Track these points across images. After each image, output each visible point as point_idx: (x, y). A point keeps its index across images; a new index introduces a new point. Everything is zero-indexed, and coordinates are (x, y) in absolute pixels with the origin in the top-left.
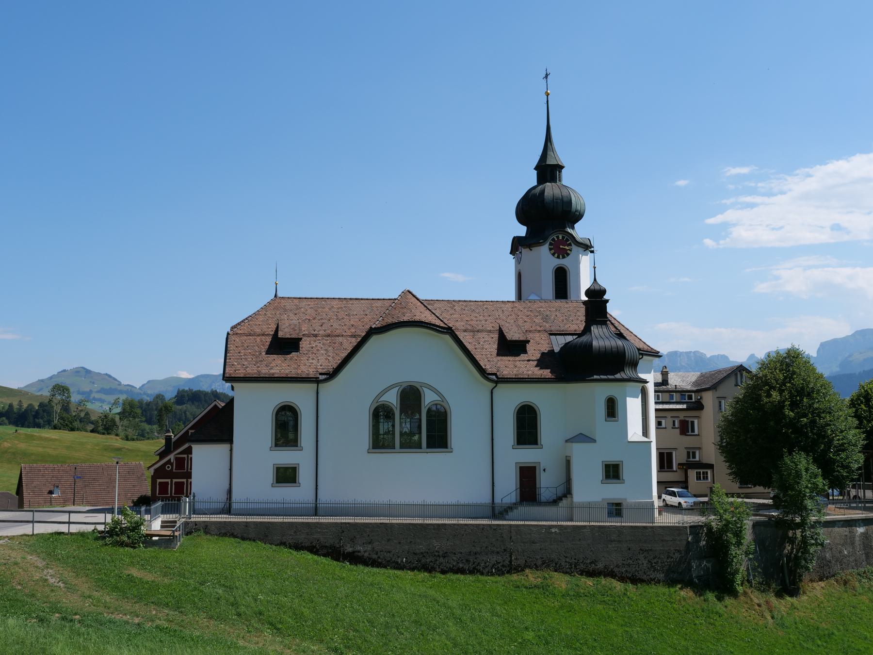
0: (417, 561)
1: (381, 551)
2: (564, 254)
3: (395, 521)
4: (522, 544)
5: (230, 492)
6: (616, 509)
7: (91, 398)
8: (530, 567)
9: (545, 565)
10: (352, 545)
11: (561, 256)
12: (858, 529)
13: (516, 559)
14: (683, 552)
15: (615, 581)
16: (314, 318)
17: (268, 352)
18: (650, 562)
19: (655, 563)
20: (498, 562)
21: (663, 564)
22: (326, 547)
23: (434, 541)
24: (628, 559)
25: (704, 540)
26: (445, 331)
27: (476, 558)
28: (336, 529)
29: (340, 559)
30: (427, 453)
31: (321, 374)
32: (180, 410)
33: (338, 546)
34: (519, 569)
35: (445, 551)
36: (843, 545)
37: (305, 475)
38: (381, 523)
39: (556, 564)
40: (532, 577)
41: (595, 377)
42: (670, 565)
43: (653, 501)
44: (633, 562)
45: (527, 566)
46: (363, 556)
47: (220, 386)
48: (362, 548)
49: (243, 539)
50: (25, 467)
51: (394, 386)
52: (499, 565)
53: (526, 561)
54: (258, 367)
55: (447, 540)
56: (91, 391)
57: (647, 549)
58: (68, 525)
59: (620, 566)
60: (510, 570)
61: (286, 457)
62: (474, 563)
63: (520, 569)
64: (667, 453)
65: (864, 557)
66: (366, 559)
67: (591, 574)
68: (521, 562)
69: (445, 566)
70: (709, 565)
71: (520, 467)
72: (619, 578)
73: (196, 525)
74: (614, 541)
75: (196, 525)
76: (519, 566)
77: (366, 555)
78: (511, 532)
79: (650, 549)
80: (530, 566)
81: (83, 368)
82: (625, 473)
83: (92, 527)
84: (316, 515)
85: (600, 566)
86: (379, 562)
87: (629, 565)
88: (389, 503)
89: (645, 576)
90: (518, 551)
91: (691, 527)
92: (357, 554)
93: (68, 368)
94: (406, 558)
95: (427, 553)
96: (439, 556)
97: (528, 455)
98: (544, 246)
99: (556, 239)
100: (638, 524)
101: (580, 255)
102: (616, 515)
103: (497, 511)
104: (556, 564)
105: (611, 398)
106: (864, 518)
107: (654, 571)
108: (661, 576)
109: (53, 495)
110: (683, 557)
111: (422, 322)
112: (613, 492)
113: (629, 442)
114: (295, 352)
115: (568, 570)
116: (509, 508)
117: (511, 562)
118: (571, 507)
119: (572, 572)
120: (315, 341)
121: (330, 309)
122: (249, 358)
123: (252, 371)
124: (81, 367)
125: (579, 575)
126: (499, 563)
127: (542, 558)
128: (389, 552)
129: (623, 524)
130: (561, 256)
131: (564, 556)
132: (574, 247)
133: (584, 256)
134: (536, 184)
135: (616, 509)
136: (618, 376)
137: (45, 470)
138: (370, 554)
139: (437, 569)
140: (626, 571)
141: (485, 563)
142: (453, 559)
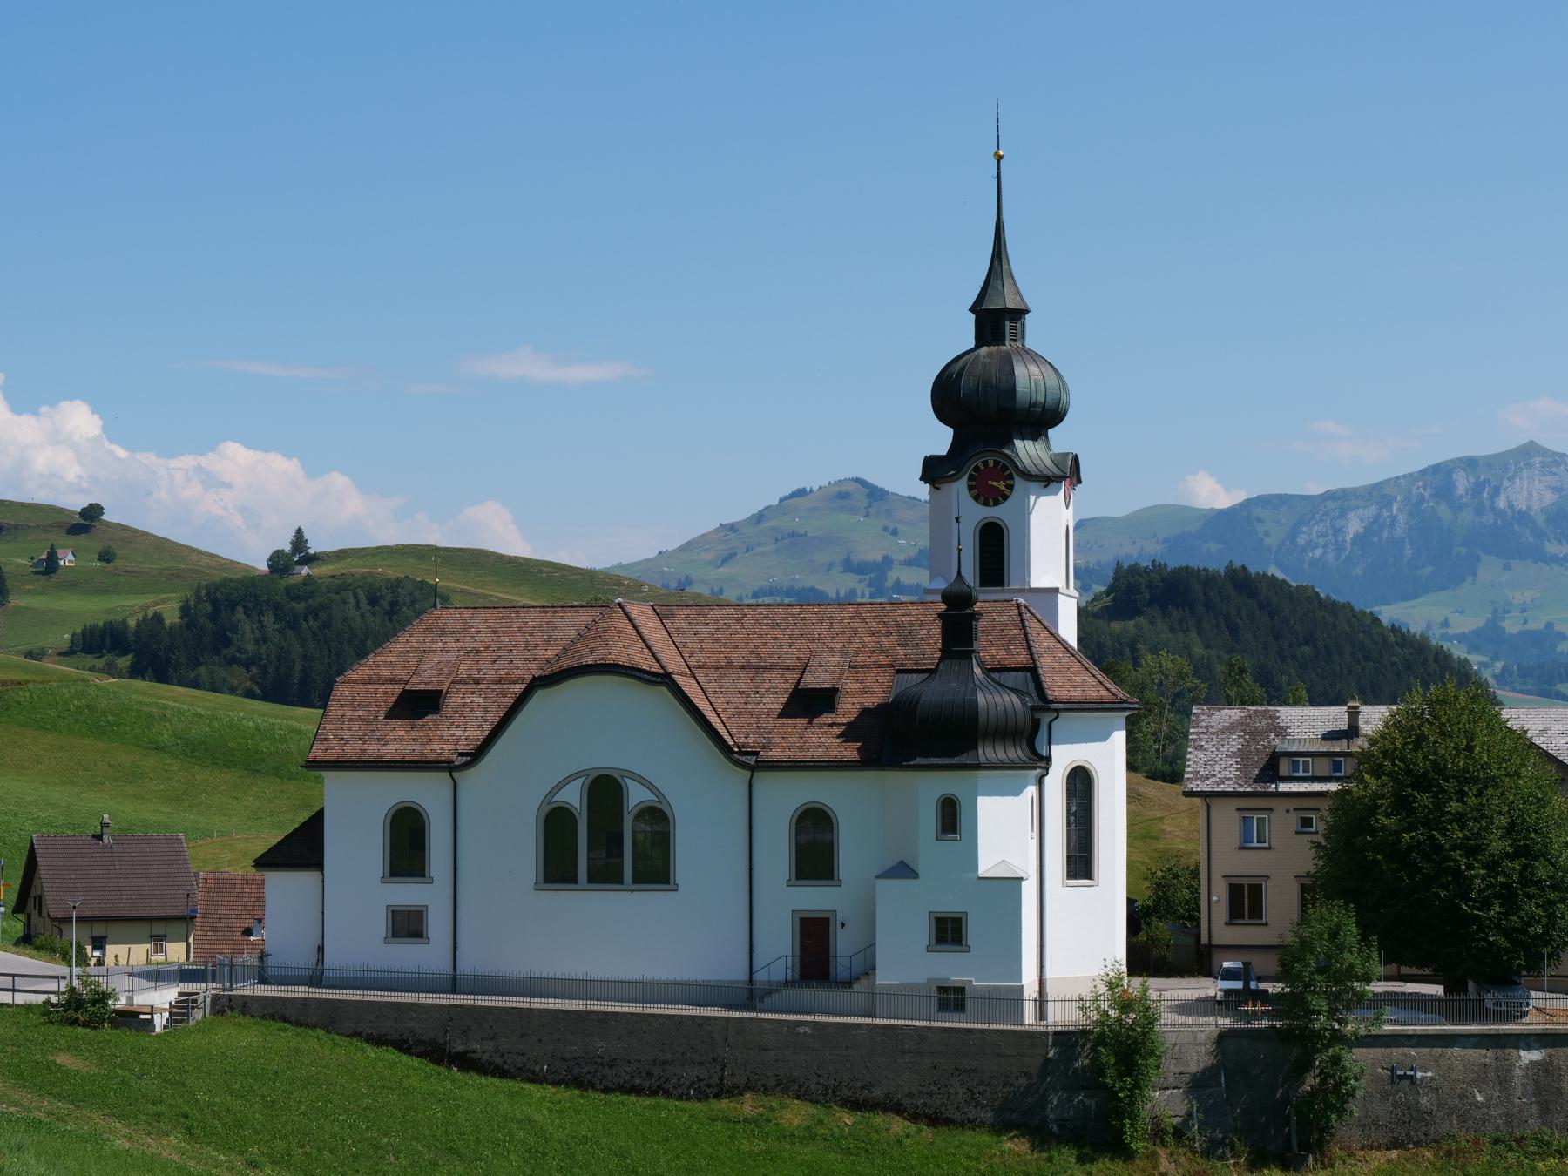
0: (566, 1071)
1: (508, 1053)
2: (999, 498)
3: (656, 1009)
4: (745, 1051)
5: (321, 949)
6: (954, 999)
7: (889, 583)
8: (754, 1090)
9: (782, 1086)
10: (465, 1042)
11: (991, 501)
12: (1522, 1053)
13: (732, 1075)
14: (1035, 1076)
15: (901, 1120)
16: (487, 648)
17: (390, 715)
18: (972, 1091)
19: (979, 1093)
20: (701, 1078)
21: (995, 1096)
22: (424, 1042)
23: (597, 1039)
24: (930, 1084)
25: (1087, 1057)
26: (659, 680)
27: (663, 1071)
28: (441, 1015)
29: (443, 1062)
30: (632, 891)
31: (461, 754)
32: (1118, 636)
33: (441, 1041)
34: (732, 1092)
35: (613, 1057)
36: (1473, 1083)
37: (437, 926)
38: (513, 1008)
39: (800, 1086)
40: (748, 1105)
41: (919, 761)
42: (1006, 1098)
43: (1023, 986)
44: (939, 1089)
45: (749, 1087)
46: (480, 1059)
47: (1324, 535)
48: (478, 1047)
49: (299, 1024)
50: (206, 879)
51: (574, 777)
52: (702, 1084)
53: (748, 1079)
54: (365, 743)
55: (619, 1039)
56: (887, 562)
57: (968, 1068)
58: (11, 993)
59: (915, 1095)
60: (719, 1092)
61: (407, 894)
62: (659, 1079)
63: (736, 1092)
64: (1250, 885)
65: (1534, 1109)
66: (484, 1064)
67: (856, 1106)
68: (740, 1080)
69: (611, 1081)
70: (1091, 1102)
71: (801, 919)
72: (909, 1115)
73: (230, 1000)
74: (910, 1052)
75: (230, 1000)
76: (735, 1086)
77: (485, 1057)
78: (727, 1030)
79: (974, 1068)
80: (754, 1088)
81: (858, 481)
82: (973, 933)
83: (43, 998)
84: (454, 992)
85: (878, 1093)
86: (504, 1070)
87: (931, 1094)
88: (529, 976)
89: (959, 1114)
90: (736, 1063)
91: (1056, 1033)
92: (471, 1055)
93: (812, 483)
94: (549, 1066)
95: (584, 1059)
96: (602, 1064)
97: (815, 898)
98: (959, 482)
99: (982, 468)
100: (958, 1025)
101: (1032, 498)
102: (954, 1008)
103: (751, 994)
104: (800, 1086)
105: (948, 798)
106: (1540, 1032)
107: (976, 1106)
108: (987, 1116)
109: (252, 938)
110: (1033, 1084)
111: (617, 665)
112: (952, 968)
113: (981, 878)
114: (432, 713)
115: (821, 1098)
116: (771, 989)
117: (721, 1079)
118: (872, 993)
119: (827, 1102)
120: (473, 693)
121: (520, 629)
122: (356, 725)
123: (351, 752)
124: (853, 480)
125: (838, 1106)
126: (702, 1080)
127: (777, 1076)
128: (522, 1055)
129: (992, 1027)
130: (991, 501)
131: (817, 1074)
132: (1019, 483)
133: (1042, 498)
134: (972, 344)
135: (952, 998)
136: (955, 761)
137: (245, 886)
138: (491, 1056)
139: (598, 1086)
140: (925, 1105)
141: (679, 1080)
142: (625, 1071)
